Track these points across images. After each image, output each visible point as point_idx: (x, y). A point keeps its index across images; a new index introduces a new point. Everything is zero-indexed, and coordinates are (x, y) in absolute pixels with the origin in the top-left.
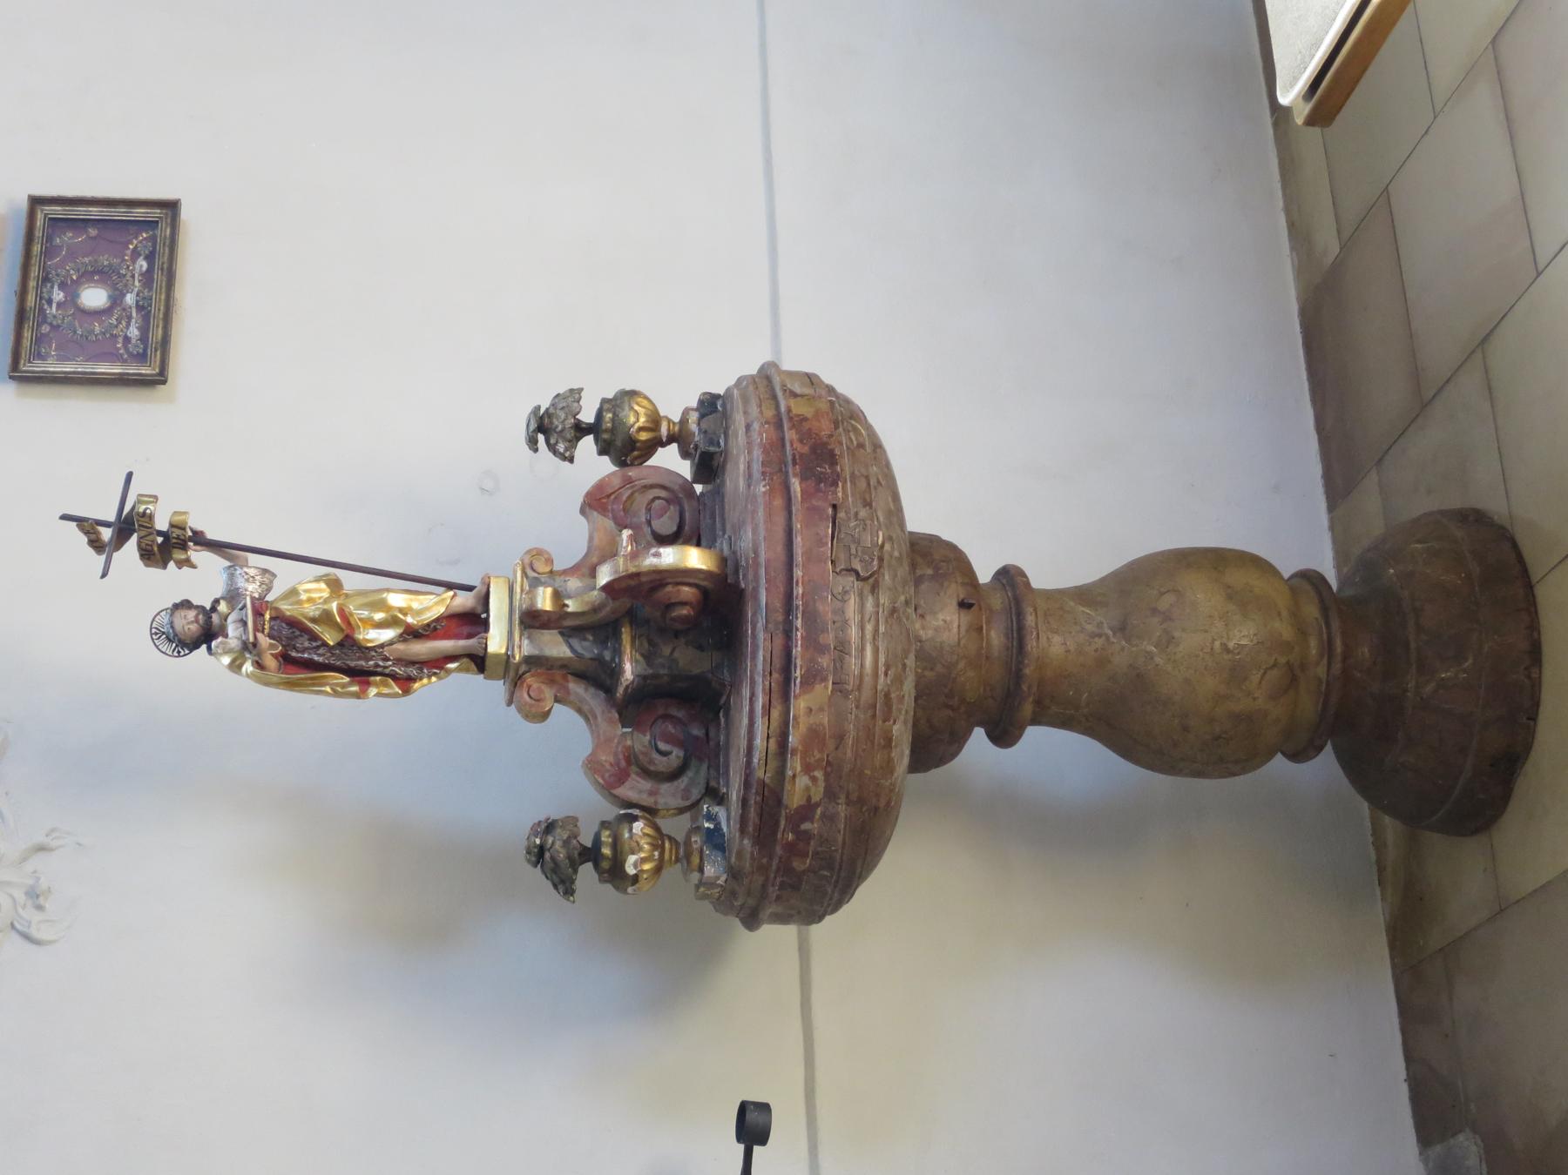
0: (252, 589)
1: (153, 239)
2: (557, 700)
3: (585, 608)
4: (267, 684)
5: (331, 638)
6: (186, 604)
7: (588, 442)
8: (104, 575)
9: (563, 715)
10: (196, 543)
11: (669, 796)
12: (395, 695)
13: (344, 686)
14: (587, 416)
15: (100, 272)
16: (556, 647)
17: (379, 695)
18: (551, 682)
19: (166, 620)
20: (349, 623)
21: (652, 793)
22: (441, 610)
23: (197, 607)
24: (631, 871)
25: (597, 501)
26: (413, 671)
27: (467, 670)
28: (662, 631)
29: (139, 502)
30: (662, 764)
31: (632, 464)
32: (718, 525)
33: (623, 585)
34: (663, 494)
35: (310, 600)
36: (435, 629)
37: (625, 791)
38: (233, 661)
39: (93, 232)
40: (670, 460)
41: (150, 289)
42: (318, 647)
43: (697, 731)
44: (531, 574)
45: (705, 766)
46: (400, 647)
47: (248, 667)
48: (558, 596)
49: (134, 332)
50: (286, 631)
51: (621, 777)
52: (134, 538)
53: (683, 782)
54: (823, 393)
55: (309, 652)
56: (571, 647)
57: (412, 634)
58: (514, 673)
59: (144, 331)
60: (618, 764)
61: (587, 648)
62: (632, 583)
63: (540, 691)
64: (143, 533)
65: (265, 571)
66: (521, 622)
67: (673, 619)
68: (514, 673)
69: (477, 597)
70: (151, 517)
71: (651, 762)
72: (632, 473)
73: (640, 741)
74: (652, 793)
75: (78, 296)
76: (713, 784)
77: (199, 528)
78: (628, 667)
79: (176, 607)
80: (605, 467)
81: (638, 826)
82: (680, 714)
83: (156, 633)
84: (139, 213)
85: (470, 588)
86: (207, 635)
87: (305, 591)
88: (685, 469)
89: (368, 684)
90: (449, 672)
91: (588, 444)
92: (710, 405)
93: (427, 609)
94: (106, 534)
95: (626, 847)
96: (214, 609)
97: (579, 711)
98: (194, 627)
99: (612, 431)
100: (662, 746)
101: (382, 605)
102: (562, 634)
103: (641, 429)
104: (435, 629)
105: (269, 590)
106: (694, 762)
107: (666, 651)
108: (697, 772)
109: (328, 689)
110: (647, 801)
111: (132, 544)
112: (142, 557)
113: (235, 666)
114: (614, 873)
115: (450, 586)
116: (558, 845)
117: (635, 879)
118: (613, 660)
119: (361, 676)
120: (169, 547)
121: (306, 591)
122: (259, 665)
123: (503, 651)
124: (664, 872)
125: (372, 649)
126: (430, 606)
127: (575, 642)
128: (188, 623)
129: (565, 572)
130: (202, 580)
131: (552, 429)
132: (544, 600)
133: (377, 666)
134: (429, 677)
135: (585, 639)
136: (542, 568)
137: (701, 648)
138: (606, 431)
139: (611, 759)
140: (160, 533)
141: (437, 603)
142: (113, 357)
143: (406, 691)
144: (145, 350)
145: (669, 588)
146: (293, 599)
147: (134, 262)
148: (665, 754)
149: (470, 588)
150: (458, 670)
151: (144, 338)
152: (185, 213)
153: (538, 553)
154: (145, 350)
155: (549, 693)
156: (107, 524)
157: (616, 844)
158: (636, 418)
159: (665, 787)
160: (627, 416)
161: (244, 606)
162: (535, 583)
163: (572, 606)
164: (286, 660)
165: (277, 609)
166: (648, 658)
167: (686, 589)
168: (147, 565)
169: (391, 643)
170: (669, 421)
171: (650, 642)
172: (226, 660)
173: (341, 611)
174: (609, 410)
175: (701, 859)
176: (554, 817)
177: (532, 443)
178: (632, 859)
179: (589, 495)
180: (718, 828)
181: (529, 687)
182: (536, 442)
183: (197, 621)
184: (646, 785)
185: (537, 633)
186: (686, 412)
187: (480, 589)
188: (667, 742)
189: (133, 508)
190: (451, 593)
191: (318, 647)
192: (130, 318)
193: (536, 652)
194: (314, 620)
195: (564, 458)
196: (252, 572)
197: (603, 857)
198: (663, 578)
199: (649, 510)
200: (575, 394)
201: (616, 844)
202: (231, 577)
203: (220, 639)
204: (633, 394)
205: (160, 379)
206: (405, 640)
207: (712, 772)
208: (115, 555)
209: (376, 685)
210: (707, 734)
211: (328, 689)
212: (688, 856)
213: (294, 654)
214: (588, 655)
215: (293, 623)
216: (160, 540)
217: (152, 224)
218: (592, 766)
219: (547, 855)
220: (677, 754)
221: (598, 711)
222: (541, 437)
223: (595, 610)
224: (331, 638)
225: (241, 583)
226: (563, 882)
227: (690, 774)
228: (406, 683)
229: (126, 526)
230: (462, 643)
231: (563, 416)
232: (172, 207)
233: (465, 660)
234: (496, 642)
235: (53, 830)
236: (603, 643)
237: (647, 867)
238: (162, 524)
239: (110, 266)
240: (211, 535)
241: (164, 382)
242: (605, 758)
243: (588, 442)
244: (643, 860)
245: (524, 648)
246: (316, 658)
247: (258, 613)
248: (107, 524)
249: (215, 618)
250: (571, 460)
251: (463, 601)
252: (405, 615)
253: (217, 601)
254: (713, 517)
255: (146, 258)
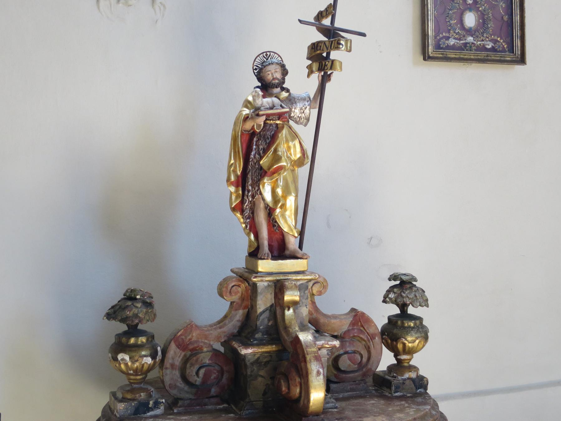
0: (296, 112)
1: (504, 51)
2: (232, 303)
3: (287, 322)
4: (235, 124)
5: (264, 162)
6: (285, 72)
7: (396, 310)
8: (300, 21)
9: (221, 307)
10: (323, 76)
11: (171, 376)
12: (231, 203)
13: (234, 171)
14: (411, 310)
15: (484, 23)
16: (263, 302)
17: (231, 193)
18: (243, 299)
19: (274, 60)
20: (274, 173)
21: (172, 366)
22: (286, 229)
23: (284, 79)
24: (120, 356)
25: (359, 319)
26: (247, 212)
27: (250, 246)
28: (275, 369)
29: (347, 41)
30: (191, 371)
31: (382, 339)
32: (346, 394)
33: (299, 350)
34: (365, 360)
35: (289, 148)
36: (274, 226)
37: (173, 348)
38: (249, 102)
39: (506, 18)
40: (387, 359)
41: (476, 50)
42: (259, 154)
43: (214, 391)
44: (311, 284)
45: (192, 397)
46: (262, 205)
47: (246, 111)
48: (295, 304)
49: (452, 42)
50: (269, 134)
51: (182, 346)
52: (325, 39)
53: (180, 384)
54: (432, 402)
55: (255, 149)
56: (264, 312)
57: (270, 212)
58: (246, 276)
59: (453, 48)
60: (191, 343)
61: (263, 322)
62: (301, 356)
63: (236, 293)
64: (327, 44)
65: (308, 120)
66: (278, 281)
67: (279, 382)
68: (246, 276)
69: (295, 251)
70: (337, 48)
71: (192, 365)
72: (378, 339)
73: (206, 358)
74: (172, 366)
75: (470, 11)
76: (180, 403)
77: (333, 78)
78: (249, 351)
79: (283, 66)
80: (380, 321)
81: (149, 361)
82: (224, 380)
83: (267, 55)
84: (518, 43)
85: (301, 247)
86: (266, 87)
87: (290, 149)
88: (382, 367)
89: (237, 187)
90: (248, 235)
91: (395, 310)
92: (421, 383)
93: (286, 221)
94: (327, 22)
95: (134, 354)
96: (283, 89)
97: (226, 317)
98: (270, 77)
99: (403, 327)
100: (202, 372)
101: (287, 192)
102: (272, 306)
103: (404, 344)
104: (274, 226)
105: (296, 122)
106: (194, 390)
107: (262, 373)
108: (187, 392)
109: (232, 162)
110: (168, 363)
111: (321, 38)
112: (313, 44)
113: (247, 104)
114: (120, 346)
115: (302, 234)
116: (135, 311)
117: (115, 359)
118: (256, 339)
119: (242, 182)
120: (320, 59)
121: (294, 145)
122: (246, 118)
123: (260, 269)
124: (124, 376)
125: (259, 188)
126: (288, 222)
127: (267, 314)
128: (273, 73)
129: (313, 303)
130: (301, 81)
131: (403, 288)
132: (289, 297)
133: (249, 191)
134: (245, 223)
135: (269, 320)
136: (315, 290)
137: (265, 394)
138: (403, 323)
139: (194, 339)
140: (328, 54)
141: (289, 226)
142: (438, 31)
143: (234, 209)
144: (442, 48)
145: (298, 380)
146: (289, 138)
147: (490, 41)
148: (197, 373)
149: (301, 247)
150: (250, 241)
151: (448, 47)
152: (518, 68)
153: (325, 286)
154: (442, 48)
155: (235, 298)
156: (332, 22)
157: (138, 347)
158: (410, 340)
159: (177, 373)
160: (412, 336)
161: (283, 107)
162: (302, 288)
163: (289, 313)
164: (252, 134)
165: (283, 127)
166: (257, 362)
167: (298, 390)
168: (308, 47)
169: (264, 200)
170: (410, 360)
171: (267, 363)
172: (250, 98)
173: (281, 168)
174: (415, 324)
175: (130, 400)
176: (156, 306)
177: (394, 277)
178: (127, 358)
179: (363, 314)
180: (152, 409)
181: (239, 286)
182: (395, 280)
183: (274, 79)
184: (178, 362)
185: (272, 290)
186: (415, 369)
187: (300, 253)
188: (205, 375)
189: (343, 37)
190: (296, 235)
191: (259, 154)
192: (460, 39)
193: (259, 290)
194: (276, 151)
195: (386, 297)
196: (307, 111)
197: (129, 339)
198: (304, 376)
199: (354, 352)
200: (425, 303)
201: (138, 347)
202: (304, 99)
203: (261, 93)
204: (426, 338)
205: (426, 57)
206: (266, 208)
207: (188, 402)
208: (314, 28)
209: (237, 191)
210: (213, 397)
211: (232, 162)
212: (132, 391)
213: (255, 139)
214: (258, 323)
215: (274, 138)
216: (325, 55)
217: (511, 50)
218: (190, 327)
219: (129, 303)
220: (198, 381)
221: (225, 329)
222: (398, 282)
223: (286, 328)
224: (264, 162)
225: (299, 105)
226: (115, 312)
227: (186, 388)
228: (239, 208)
229: (333, 35)
230: (266, 243)
231: (412, 296)
232: (522, 60)
233: (256, 244)
234: (265, 265)
235: (164, 6)
236: (267, 332)
237: (123, 366)
238: (334, 55)
239: (488, 28)
240: (328, 85)
241: (425, 59)
242: (195, 335)
243: (396, 310)
244: (126, 365)
245: (262, 283)
246: (253, 153)
247: (280, 116)
248: (332, 22)
249: (277, 90)
250: (384, 301)
251: (292, 243)
252: (281, 207)
253: (288, 91)
254: (352, 390)
255: (493, 47)
